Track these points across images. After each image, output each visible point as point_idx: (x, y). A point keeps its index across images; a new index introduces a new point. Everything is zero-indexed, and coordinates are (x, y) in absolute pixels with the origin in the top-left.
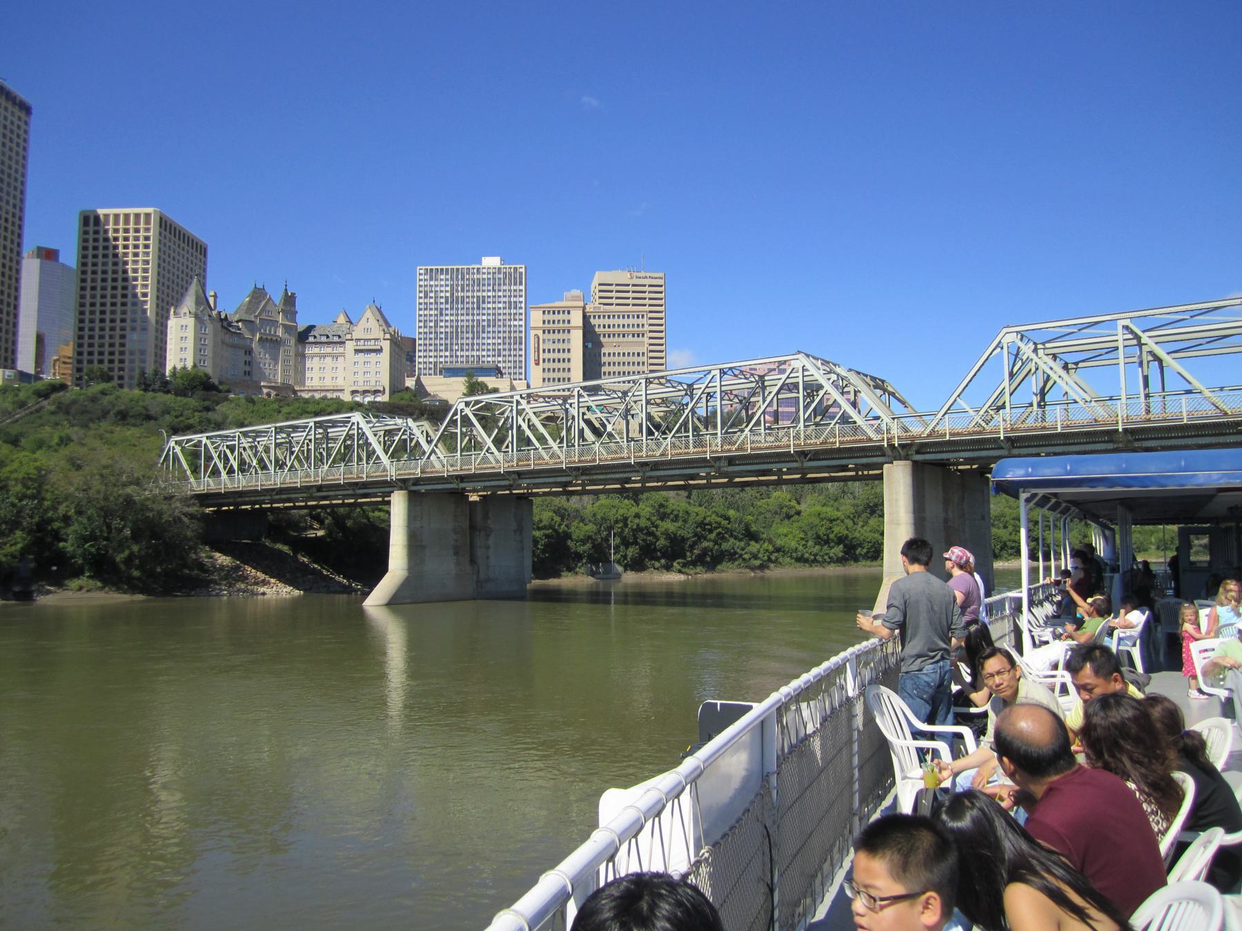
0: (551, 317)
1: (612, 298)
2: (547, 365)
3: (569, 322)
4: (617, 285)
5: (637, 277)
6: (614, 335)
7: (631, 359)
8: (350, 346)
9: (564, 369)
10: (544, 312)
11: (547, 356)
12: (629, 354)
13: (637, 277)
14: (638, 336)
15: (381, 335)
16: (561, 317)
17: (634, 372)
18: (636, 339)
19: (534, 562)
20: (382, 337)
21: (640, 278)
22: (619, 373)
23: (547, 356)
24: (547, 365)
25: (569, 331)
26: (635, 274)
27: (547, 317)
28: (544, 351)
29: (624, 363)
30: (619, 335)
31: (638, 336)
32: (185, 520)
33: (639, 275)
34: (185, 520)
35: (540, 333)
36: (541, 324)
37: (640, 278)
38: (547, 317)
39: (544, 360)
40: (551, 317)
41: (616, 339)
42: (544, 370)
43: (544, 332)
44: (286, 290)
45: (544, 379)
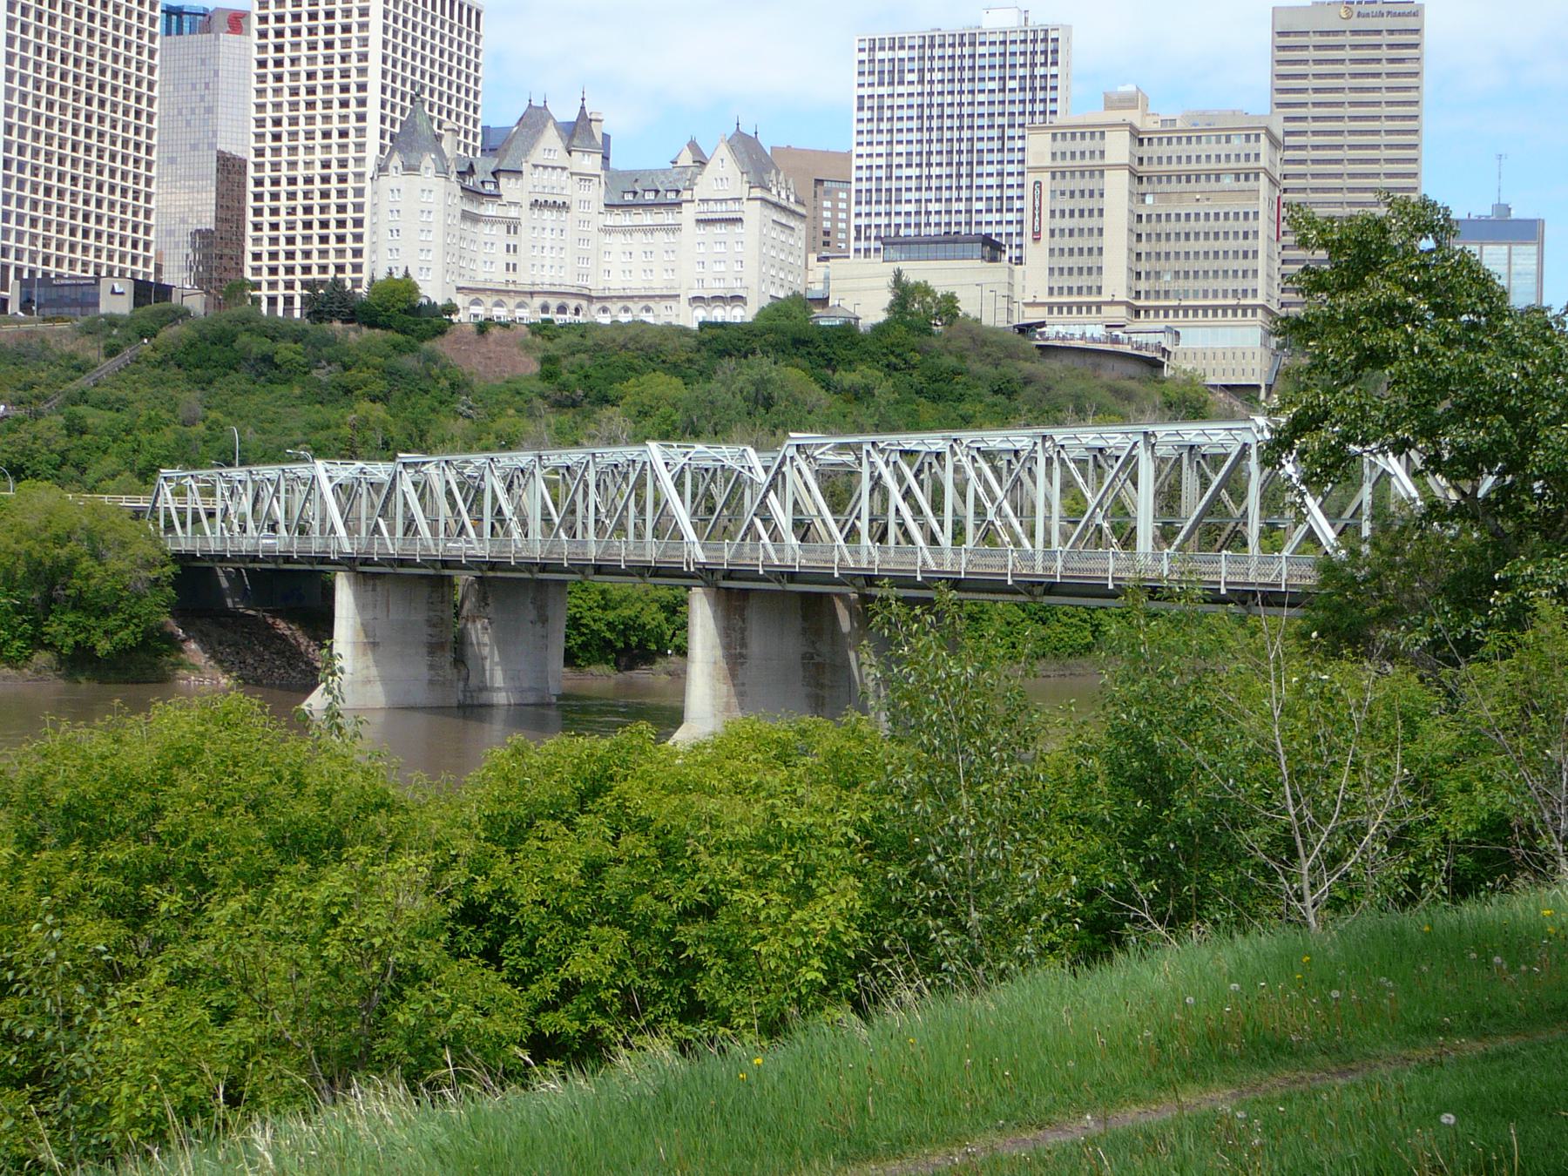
0: (1069, 146)
1: (1305, 62)
2: (1059, 242)
3: (1102, 153)
4: (1322, 33)
5: (1359, 15)
6: (1198, 178)
7: (1231, 225)
8: (689, 213)
9: (1090, 250)
10: (1054, 136)
11: (1059, 223)
12: (1217, 215)
13: (1359, 15)
14: (1247, 178)
15: (742, 190)
16: (1087, 144)
17: (1070, 289)
18: (1242, 184)
19: (331, 637)
20: (745, 197)
21: (1367, 15)
22: (1236, 253)
23: (1059, 223)
24: (1059, 242)
25: (1102, 173)
26: (1356, 8)
27: (1060, 146)
28: (1053, 212)
29: (1216, 235)
30: (1179, 178)
31: (1247, 178)
32: (1366, 494)
33: (1365, 8)
34: (1366, 494)
35: (1045, 178)
36: (1048, 162)
37: (1367, 15)
38: (1060, 146)
39: (1052, 233)
40: (1069, 146)
41: (1203, 185)
42: (1052, 251)
43: (1053, 176)
44: (583, 108)
45: (1051, 270)
